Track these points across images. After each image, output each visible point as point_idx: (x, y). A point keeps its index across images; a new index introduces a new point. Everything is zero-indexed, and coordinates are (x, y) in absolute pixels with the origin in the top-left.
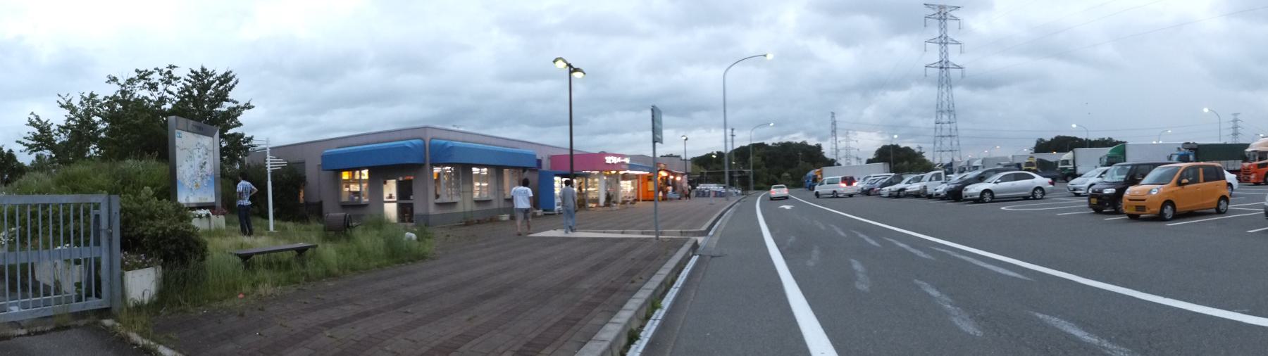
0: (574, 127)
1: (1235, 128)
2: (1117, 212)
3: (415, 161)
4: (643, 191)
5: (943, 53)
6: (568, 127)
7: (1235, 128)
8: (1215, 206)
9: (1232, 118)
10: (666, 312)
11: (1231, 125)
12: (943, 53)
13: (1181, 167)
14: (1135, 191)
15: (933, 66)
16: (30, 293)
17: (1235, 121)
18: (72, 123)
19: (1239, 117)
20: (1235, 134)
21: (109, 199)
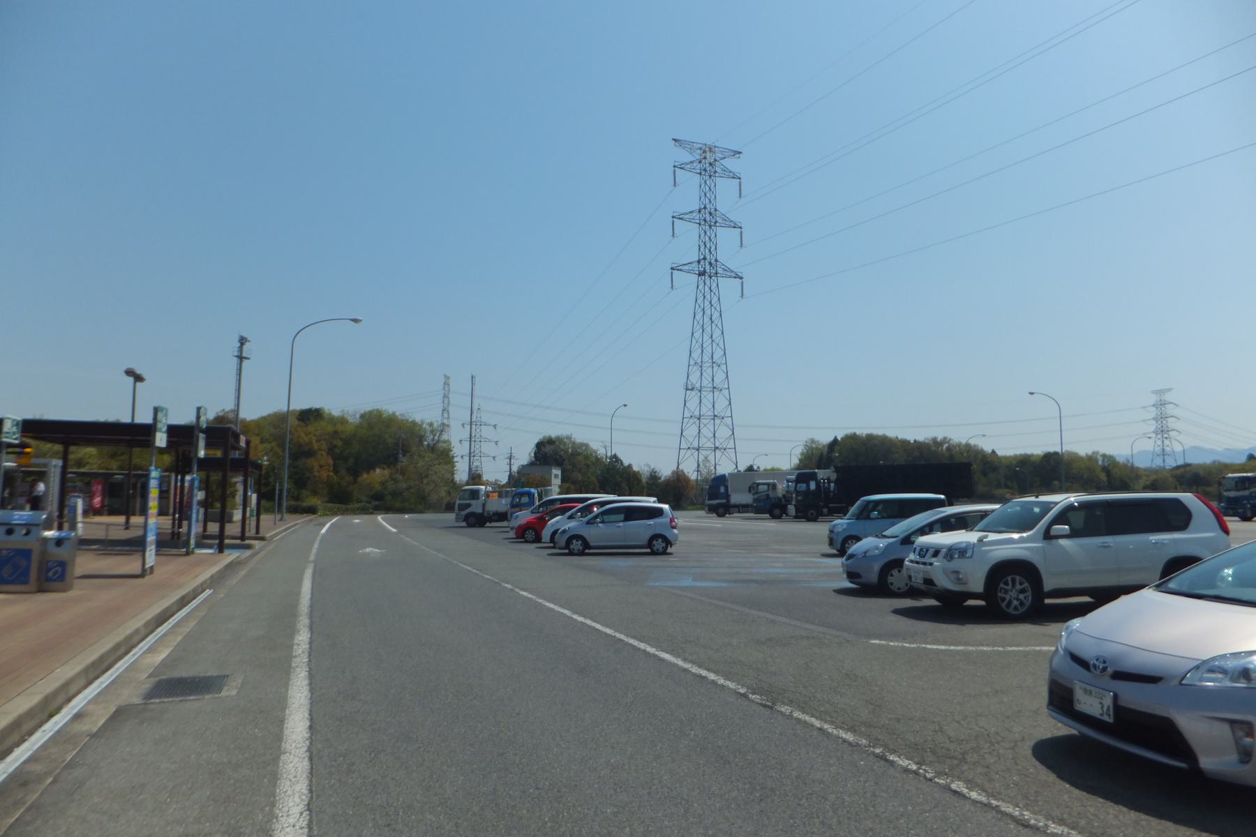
0: (1063, 432)
1: (1161, 418)
2: (538, 539)
3: (212, 672)
4: (284, 526)
5: (707, 193)
6: (1060, 433)
7: (1161, 418)
8: (143, 525)
9: (1153, 399)
10: (674, 663)
11: (1153, 412)
12: (707, 193)
13: (1056, 503)
14: (1163, 540)
15: (686, 267)
16: (293, 503)
17: (1161, 404)
18: (958, 448)
19: (1168, 397)
20: (1162, 431)
21: (672, 273)
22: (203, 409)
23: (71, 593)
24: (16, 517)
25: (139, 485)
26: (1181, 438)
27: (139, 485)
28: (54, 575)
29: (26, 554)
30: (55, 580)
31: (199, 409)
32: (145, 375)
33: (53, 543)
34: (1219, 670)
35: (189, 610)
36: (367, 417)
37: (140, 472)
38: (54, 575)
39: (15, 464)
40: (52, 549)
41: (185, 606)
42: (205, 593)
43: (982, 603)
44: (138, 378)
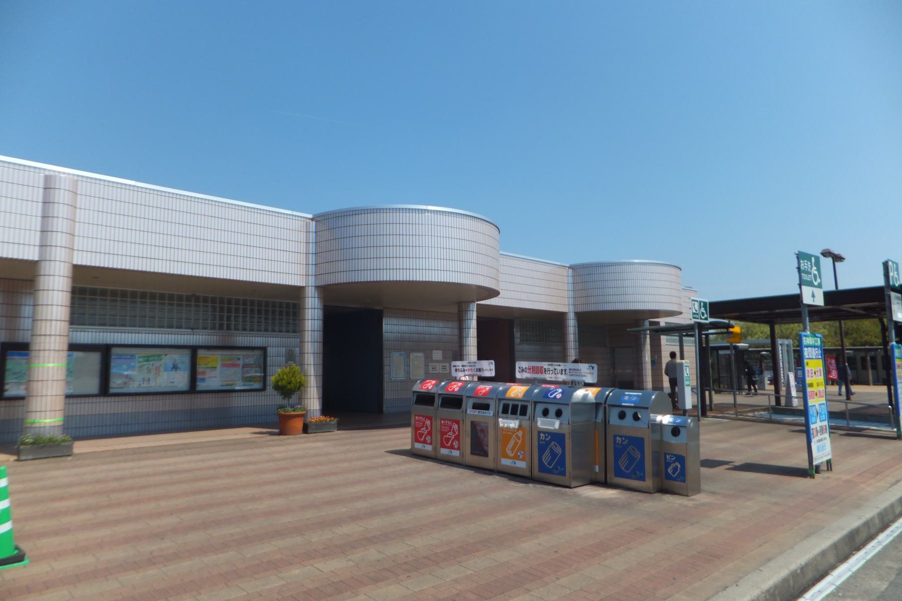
22: (890, 263)
23: (701, 498)
24: (626, 398)
25: (868, 358)
26: (318, 416)
27: (868, 358)
28: (674, 473)
29: (639, 443)
30: (675, 479)
31: (886, 265)
32: (843, 255)
33: (669, 430)
34: (711, 326)
35: (891, 539)
36: (771, 591)
37: (868, 347)
38: (674, 473)
39: (747, 345)
40: (668, 437)
41: (858, 549)
42: (888, 531)
43: (703, 332)
44: (837, 258)
